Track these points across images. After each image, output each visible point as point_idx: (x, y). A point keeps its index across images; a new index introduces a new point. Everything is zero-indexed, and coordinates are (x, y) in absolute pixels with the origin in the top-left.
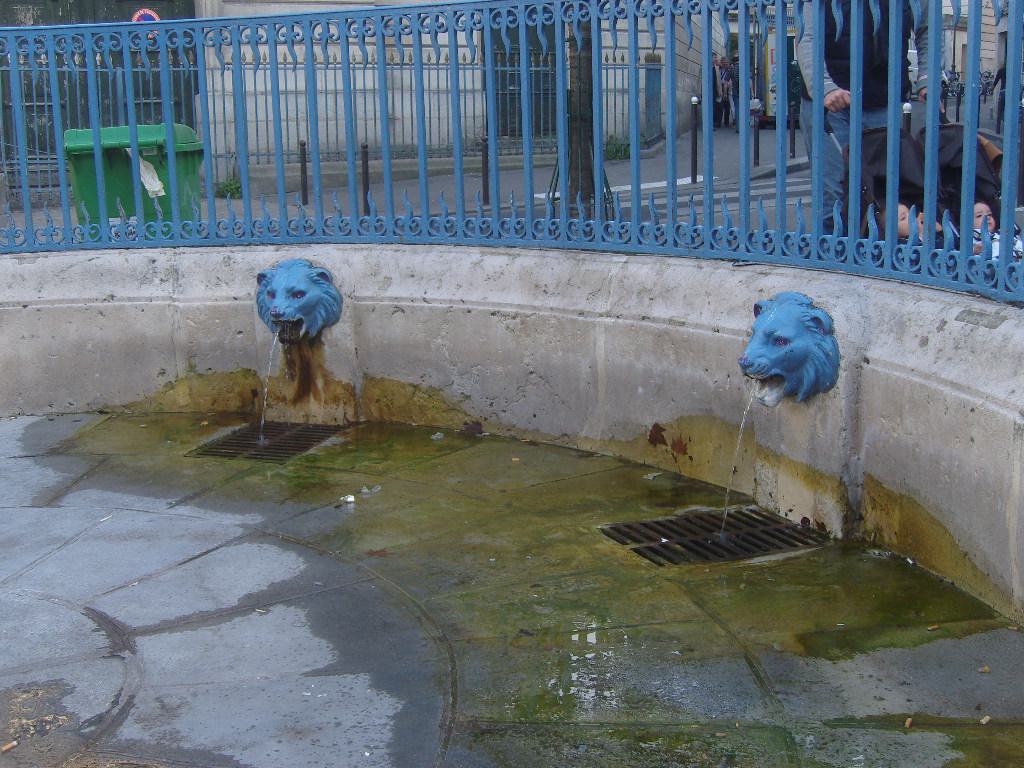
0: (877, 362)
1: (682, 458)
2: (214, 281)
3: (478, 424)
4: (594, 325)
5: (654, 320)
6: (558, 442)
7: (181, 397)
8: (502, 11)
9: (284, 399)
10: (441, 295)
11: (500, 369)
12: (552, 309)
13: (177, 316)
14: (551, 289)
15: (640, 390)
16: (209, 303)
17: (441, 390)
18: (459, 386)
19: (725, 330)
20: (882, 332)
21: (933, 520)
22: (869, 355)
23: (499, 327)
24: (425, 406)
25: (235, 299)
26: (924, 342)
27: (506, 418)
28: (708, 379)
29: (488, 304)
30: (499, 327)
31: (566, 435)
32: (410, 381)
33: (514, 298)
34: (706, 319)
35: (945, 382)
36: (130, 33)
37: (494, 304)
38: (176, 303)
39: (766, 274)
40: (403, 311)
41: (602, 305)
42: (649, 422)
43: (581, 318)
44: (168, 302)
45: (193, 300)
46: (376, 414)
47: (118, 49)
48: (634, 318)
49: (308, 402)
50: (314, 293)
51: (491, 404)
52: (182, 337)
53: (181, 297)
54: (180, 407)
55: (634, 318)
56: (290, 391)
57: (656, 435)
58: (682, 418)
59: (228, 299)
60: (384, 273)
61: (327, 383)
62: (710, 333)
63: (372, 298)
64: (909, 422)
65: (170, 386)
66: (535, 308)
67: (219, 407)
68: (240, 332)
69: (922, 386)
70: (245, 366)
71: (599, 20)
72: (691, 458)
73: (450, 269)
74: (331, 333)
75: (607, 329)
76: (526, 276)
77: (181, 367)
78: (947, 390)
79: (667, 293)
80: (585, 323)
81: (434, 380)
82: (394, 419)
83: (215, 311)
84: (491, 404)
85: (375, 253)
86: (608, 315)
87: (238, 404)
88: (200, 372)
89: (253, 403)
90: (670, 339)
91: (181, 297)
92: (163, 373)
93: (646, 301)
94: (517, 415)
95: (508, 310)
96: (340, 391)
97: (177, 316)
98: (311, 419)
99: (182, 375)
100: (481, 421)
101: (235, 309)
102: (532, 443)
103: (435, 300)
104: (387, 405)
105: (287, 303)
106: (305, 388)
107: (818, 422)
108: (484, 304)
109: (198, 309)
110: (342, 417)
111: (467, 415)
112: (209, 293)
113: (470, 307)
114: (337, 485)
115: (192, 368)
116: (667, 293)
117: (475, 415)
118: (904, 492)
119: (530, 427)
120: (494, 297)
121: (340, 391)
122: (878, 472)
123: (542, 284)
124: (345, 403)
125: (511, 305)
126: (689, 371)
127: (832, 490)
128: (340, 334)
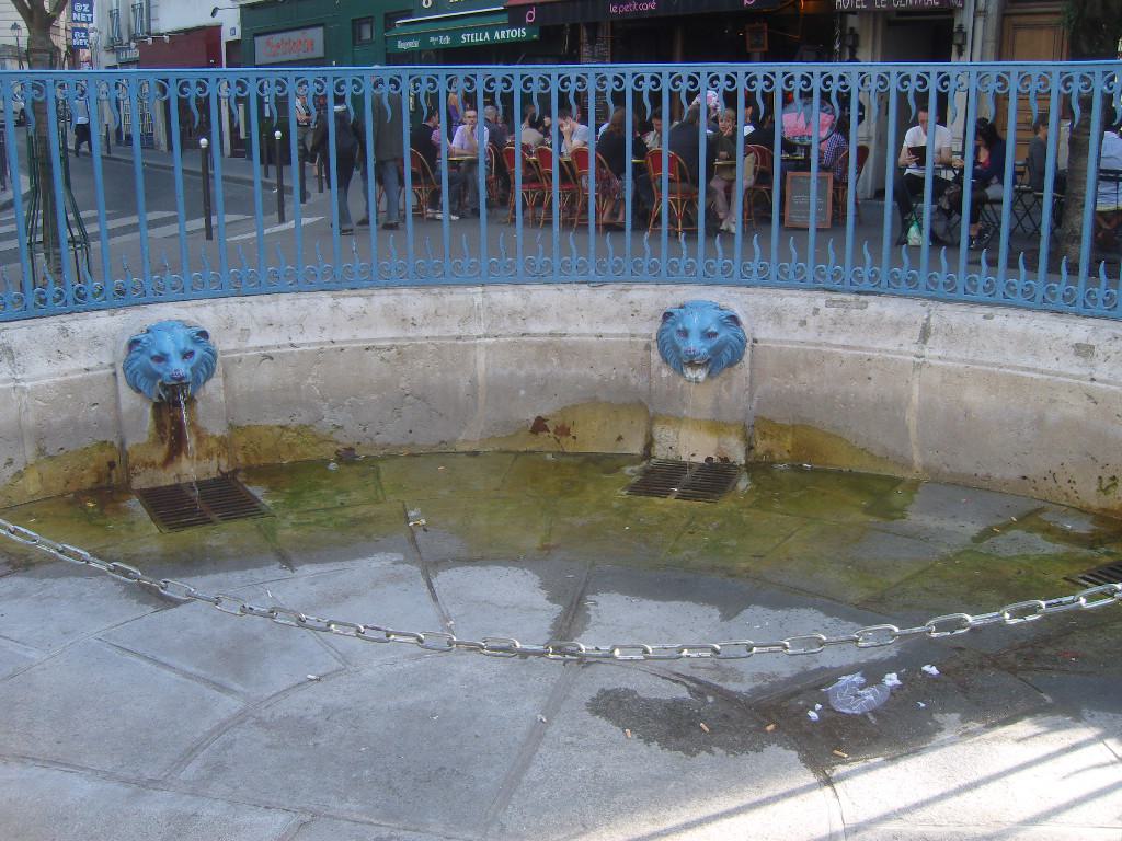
0: (762, 341)
1: (564, 440)
2: (56, 354)
3: (351, 449)
4: (475, 346)
5: (535, 335)
6: (435, 450)
7: (32, 485)
8: (191, 81)
9: (153, 464)
10: (309, 338)
11: (374, 397)
12: (427, 338)
13: (25, 398)
14: (419, 322)
15: (522, 392)
16: (58, 379)
17: (311, 425)
18: (329, 418)
19: (607, 335)
20: (760, 320)
21: (829, 435)
22: (757, 337)
23: (373, 359)
24: (294, 444)
25: (87, 370)
26: (803, 323)
27: (379, 439)
28: (593, 373)
29: (357, 341)
30: (373, 359)
31: (443, 442)
32: (278, 423)
33: (384, 333)
34: (585, 328)
35: (837, 346)
36: (899, 74)
37: (365, 341)
38: (23, 384)
39: (627, 291)
40: (272, 358)
41: (477, 329)
42: (531, 417)
43: (460, 342)
44: (12, 384)
45: (38, 378)
46: (242, 460)
47: (435, 91)
48: (513, 335)
49: (180, 461)
50: (724, 334)
51: (364, 430)
52: (30, 420)
53: (25, 376)
54: (32, 496)
55: (513, 335)
56: (159, 455)
57: (539, 426)
58: (566, 407)
59: (79, 371)
60: (240, 325)
61: (200, 439)
62: (595, 339)
63: (235, 351)
64: (803, 376)
65: (19, 475)
66: (409, 338)
67: (72, 487)
68: (94, 404)
69: (815, 352)
70: (102, 439)
71: (448, 93)
72: (575, 438)
73: (309, 314)
74: (204, 391)
75: (488, 347)
76: (388, 313)
77: (29, 452)
78: (840, 350)
79: (538, 313)
80: (464, 345)
81: (304, 418)
82: (262, 462)
83: (68, 387)
84: (364, 430)
85: (223, 307)
86: (486, 336)
87: (94, 479)
88: (51, 454)
89: (110, 476)
90: (554, 347)
91: (25, 376)
92: (10, 462)
93: (519, 321)
94: (392, 434)
95: (383, 344)
96: (213, 444)
97: (25, 398)
98: (182, 478)
99: (31, 461)
100: (354, 446)
101: (89, 380)
102: (412, 455)
103: (302, 344)
104: (254, 450)
105: (702, 344)
106: (177, 447)
107: (724, 390)
108: (357, 341)
109: (48, 386)
110: (215, 470)
111: (338, 443)
112: (56, 368)
113: (343, 346)
114: (750, 507)
115: (41, 451)
116: (538, 313)
117: (348, 442)
118: (797, 422)
119: (406, 442)
120: (363, 334)
121: (213, 444)
122: (768, 414)
123: (409, 317)
124: (219, 456)
125: (384, 339)
126: (573, 371)
127: (737, 433)
128: (213, 388)
